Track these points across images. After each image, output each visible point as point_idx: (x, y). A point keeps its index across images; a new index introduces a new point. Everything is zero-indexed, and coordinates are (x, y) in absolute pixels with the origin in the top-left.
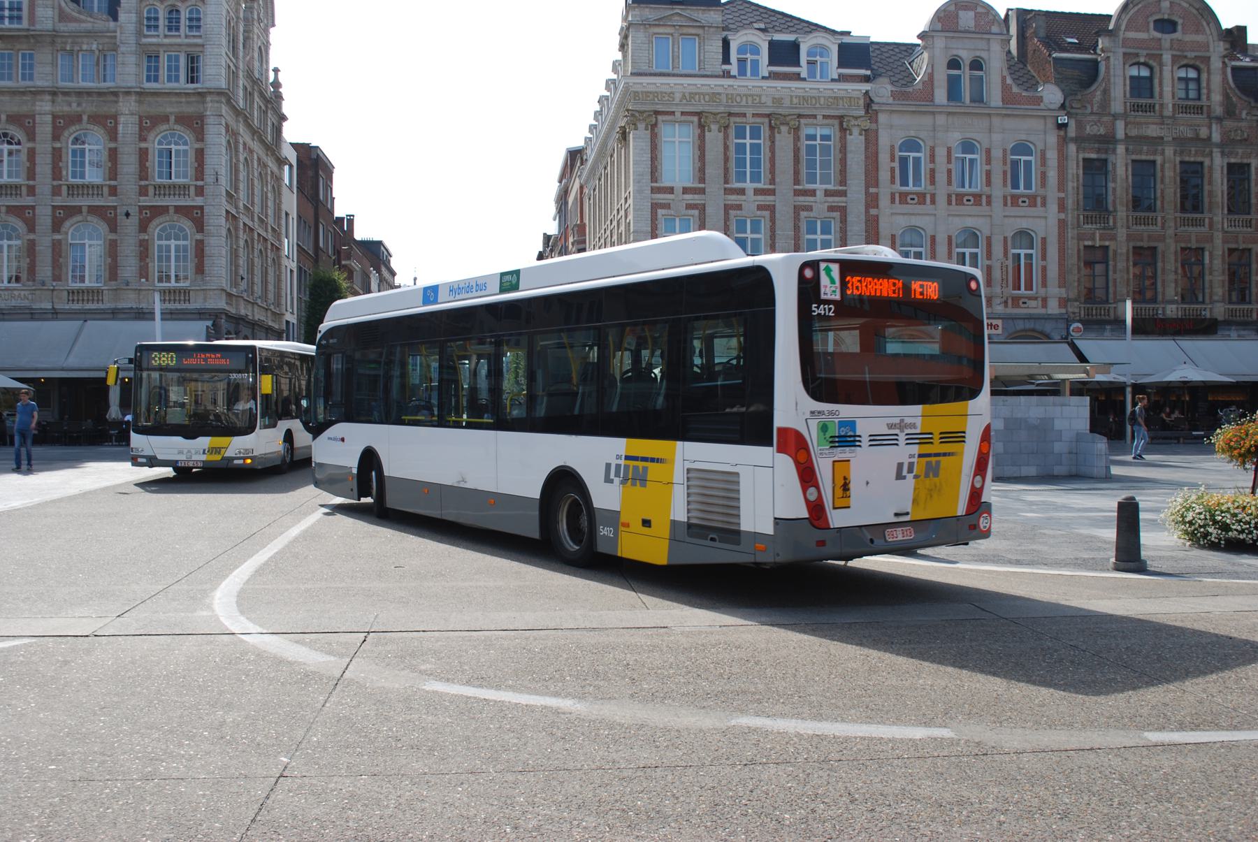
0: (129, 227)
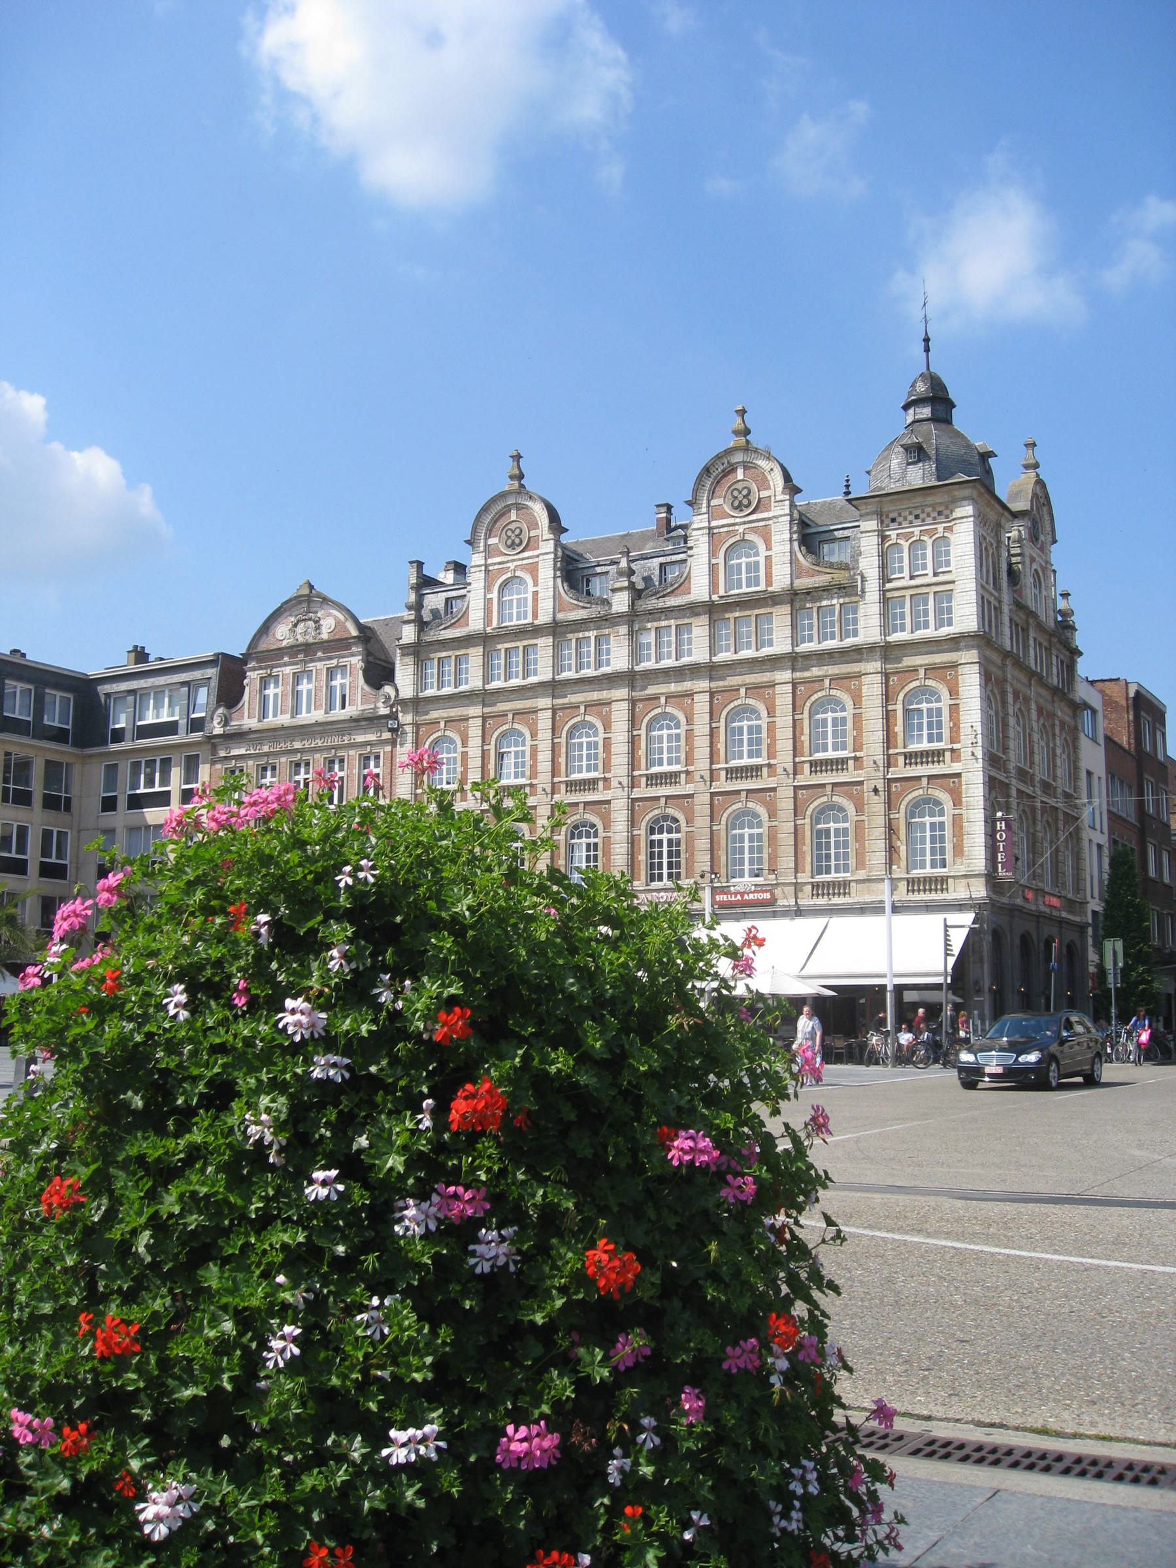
0: (877, 805)
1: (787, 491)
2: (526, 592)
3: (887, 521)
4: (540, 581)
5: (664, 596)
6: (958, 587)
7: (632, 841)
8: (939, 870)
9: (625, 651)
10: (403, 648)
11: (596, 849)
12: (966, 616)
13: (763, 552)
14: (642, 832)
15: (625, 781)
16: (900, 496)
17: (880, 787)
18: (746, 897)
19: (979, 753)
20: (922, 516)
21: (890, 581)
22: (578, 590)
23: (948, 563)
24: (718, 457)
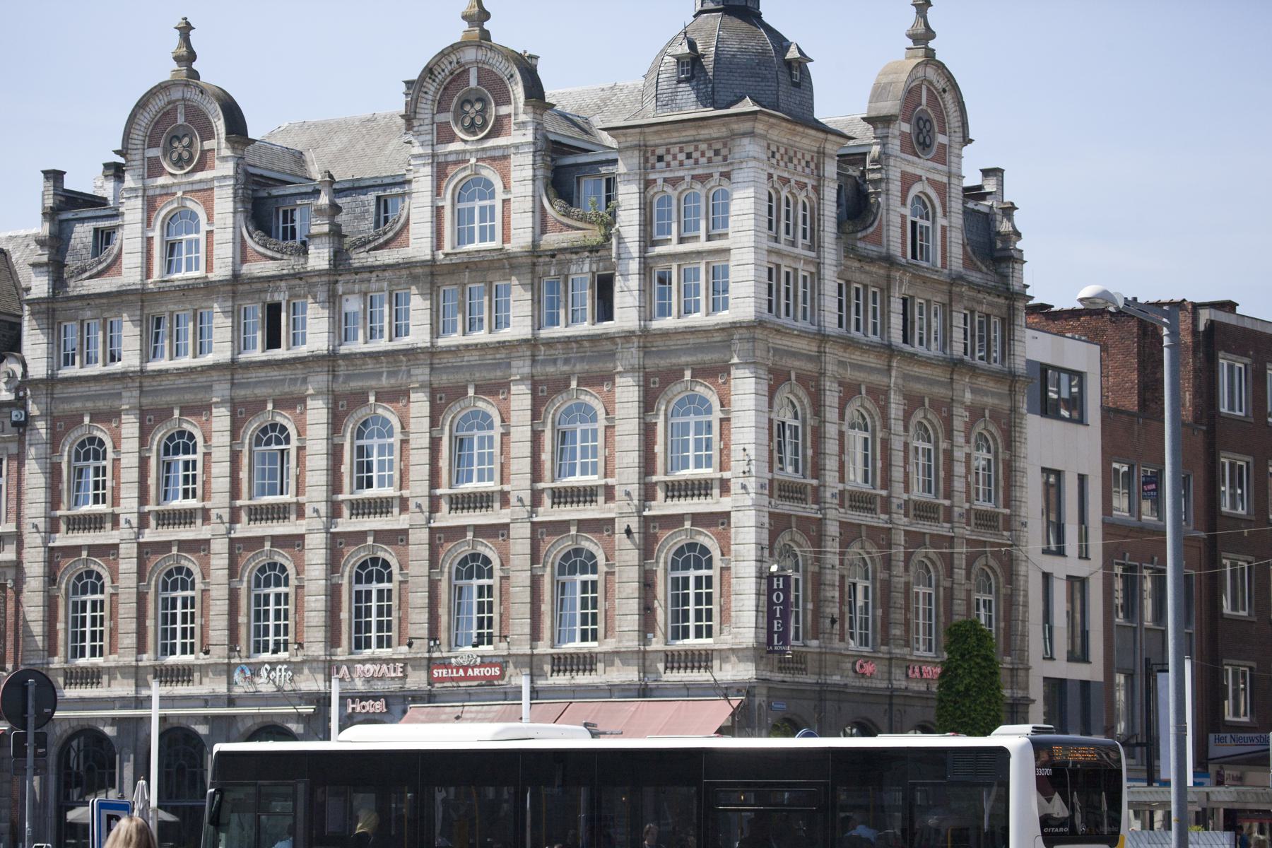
0: (628, 554)
1: (530, 109)
2: (197, 231)
3: (652, 160)
4: (216, 217)
5: (375, 248)
6: (735, 258)
7: (333, 593)
8: (385, 650)
9: (324, 325)
10: (31, 302)
11: (709, 585)
12: (743, 303)
13: (500, 195)
14: (345, 581)
15: (323, 508)
16: (667, 127)
17: (635, 527)
18: (470, 672)
19: (752, 483)
20: (695, 155)
21: (655, 243)
22: (268, 233)
23: (726, 225)
24: (443, 54)
